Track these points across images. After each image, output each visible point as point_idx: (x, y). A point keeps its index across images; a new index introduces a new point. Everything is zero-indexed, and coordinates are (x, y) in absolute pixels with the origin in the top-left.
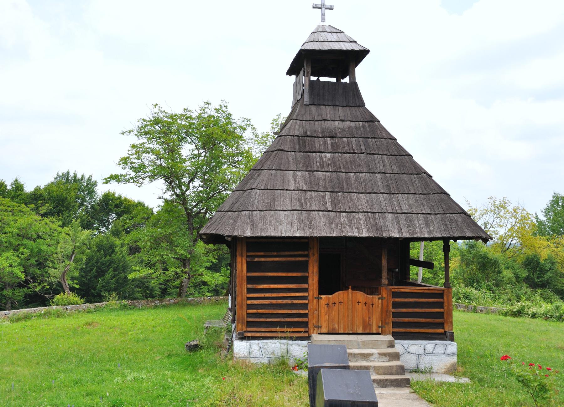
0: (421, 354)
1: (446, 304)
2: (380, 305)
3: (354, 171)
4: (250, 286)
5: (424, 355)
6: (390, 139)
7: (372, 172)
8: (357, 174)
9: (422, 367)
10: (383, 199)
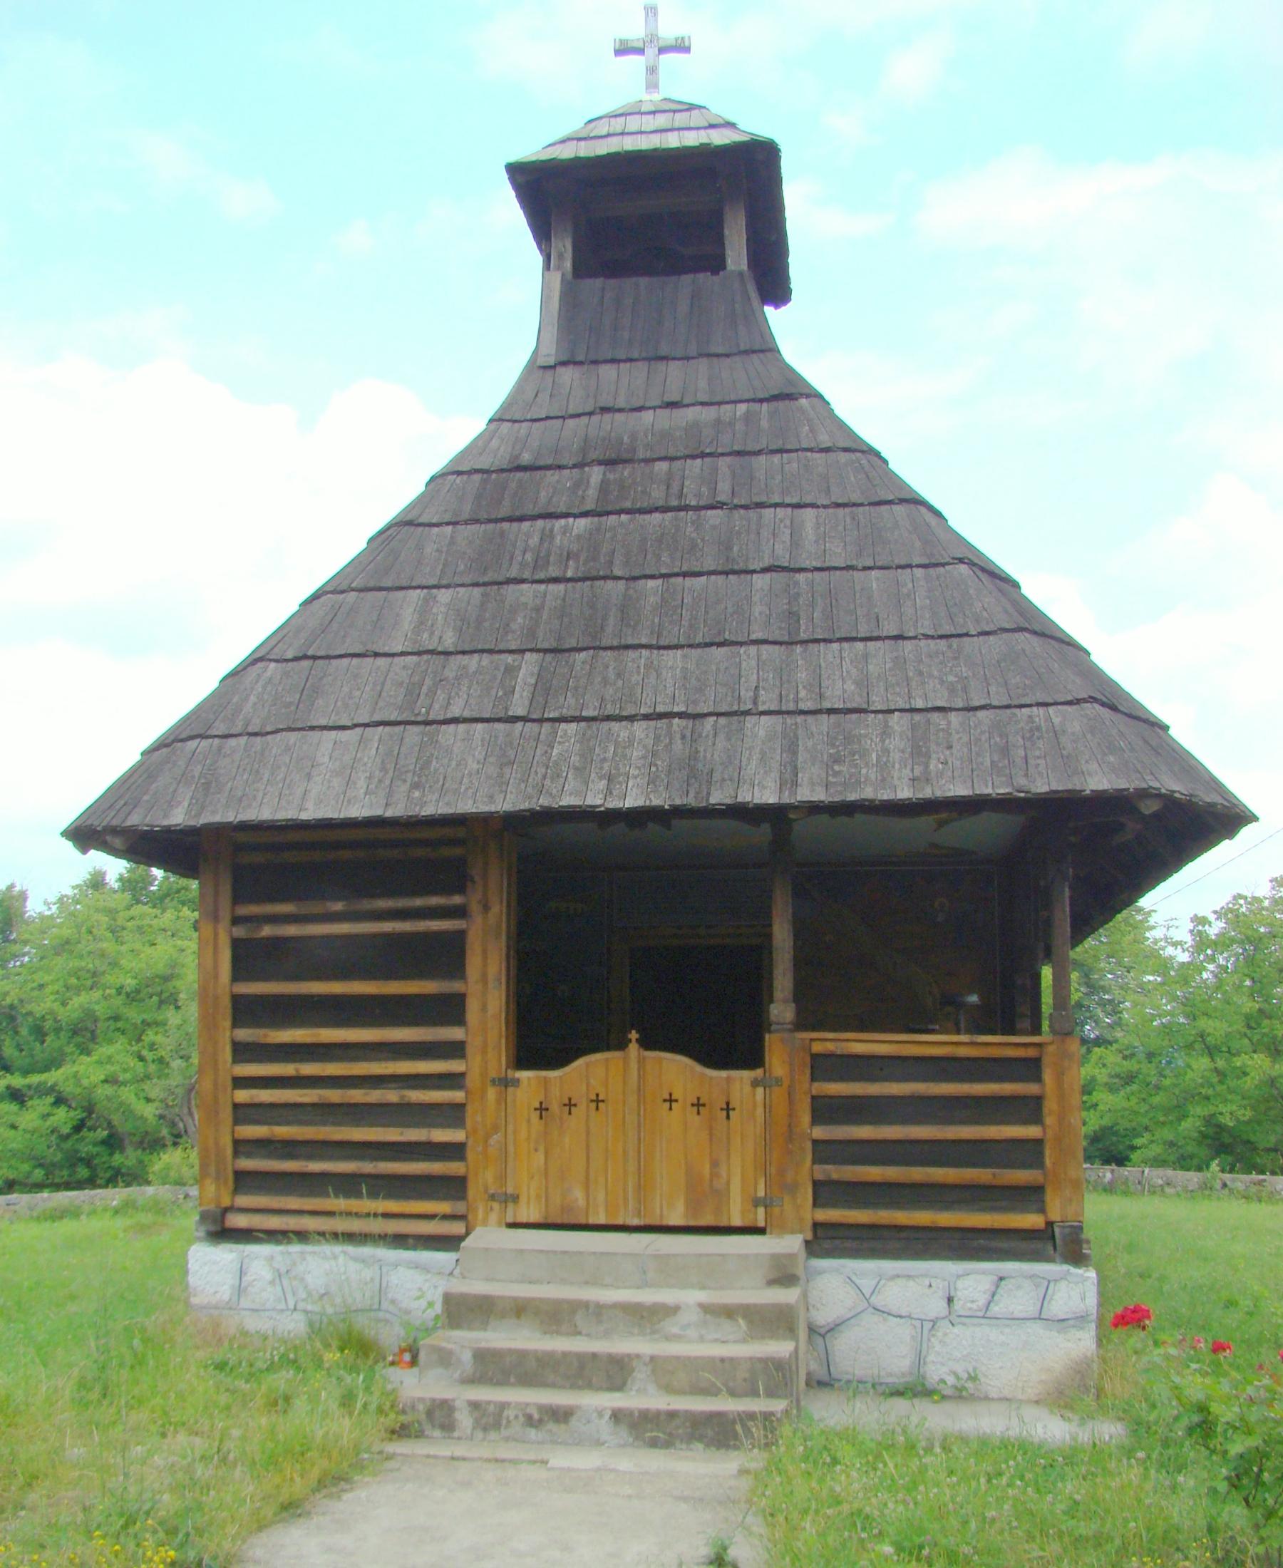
0: (932, 1315)
1: (1050, 1105)
2: (760, 1110)
3: (663, 571)
4: (244, 1034)
5: (946, 1321)
6: (846, 450)
7: (736, 567)
8: (673, 580)
9: (936, 1372)
10: (753, 663)
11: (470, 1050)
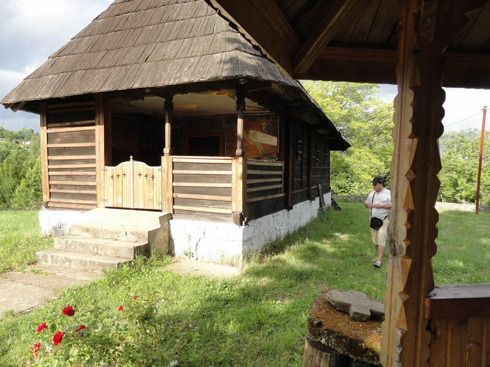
11: (97, 161)
